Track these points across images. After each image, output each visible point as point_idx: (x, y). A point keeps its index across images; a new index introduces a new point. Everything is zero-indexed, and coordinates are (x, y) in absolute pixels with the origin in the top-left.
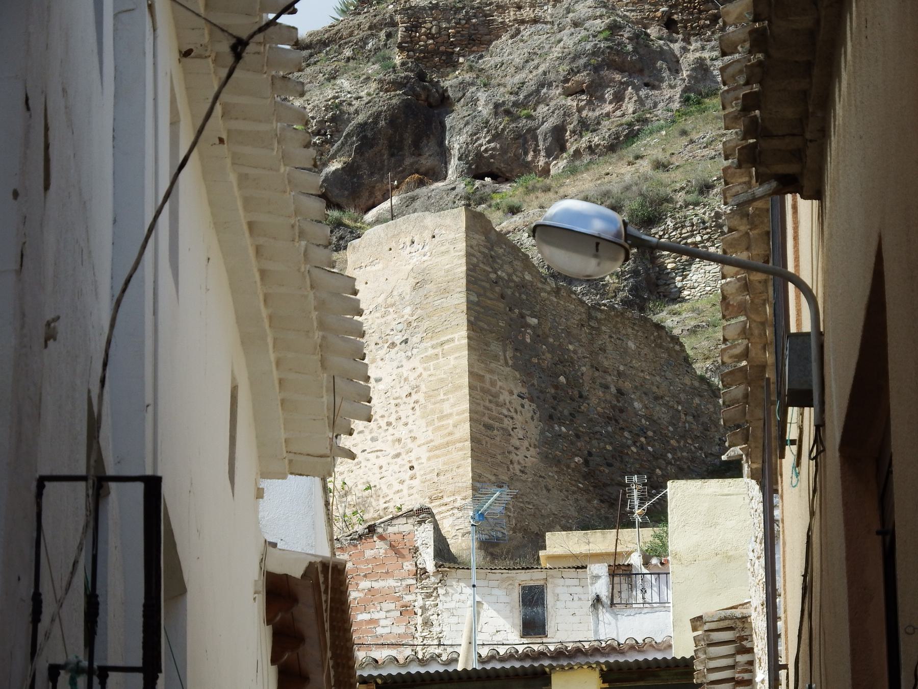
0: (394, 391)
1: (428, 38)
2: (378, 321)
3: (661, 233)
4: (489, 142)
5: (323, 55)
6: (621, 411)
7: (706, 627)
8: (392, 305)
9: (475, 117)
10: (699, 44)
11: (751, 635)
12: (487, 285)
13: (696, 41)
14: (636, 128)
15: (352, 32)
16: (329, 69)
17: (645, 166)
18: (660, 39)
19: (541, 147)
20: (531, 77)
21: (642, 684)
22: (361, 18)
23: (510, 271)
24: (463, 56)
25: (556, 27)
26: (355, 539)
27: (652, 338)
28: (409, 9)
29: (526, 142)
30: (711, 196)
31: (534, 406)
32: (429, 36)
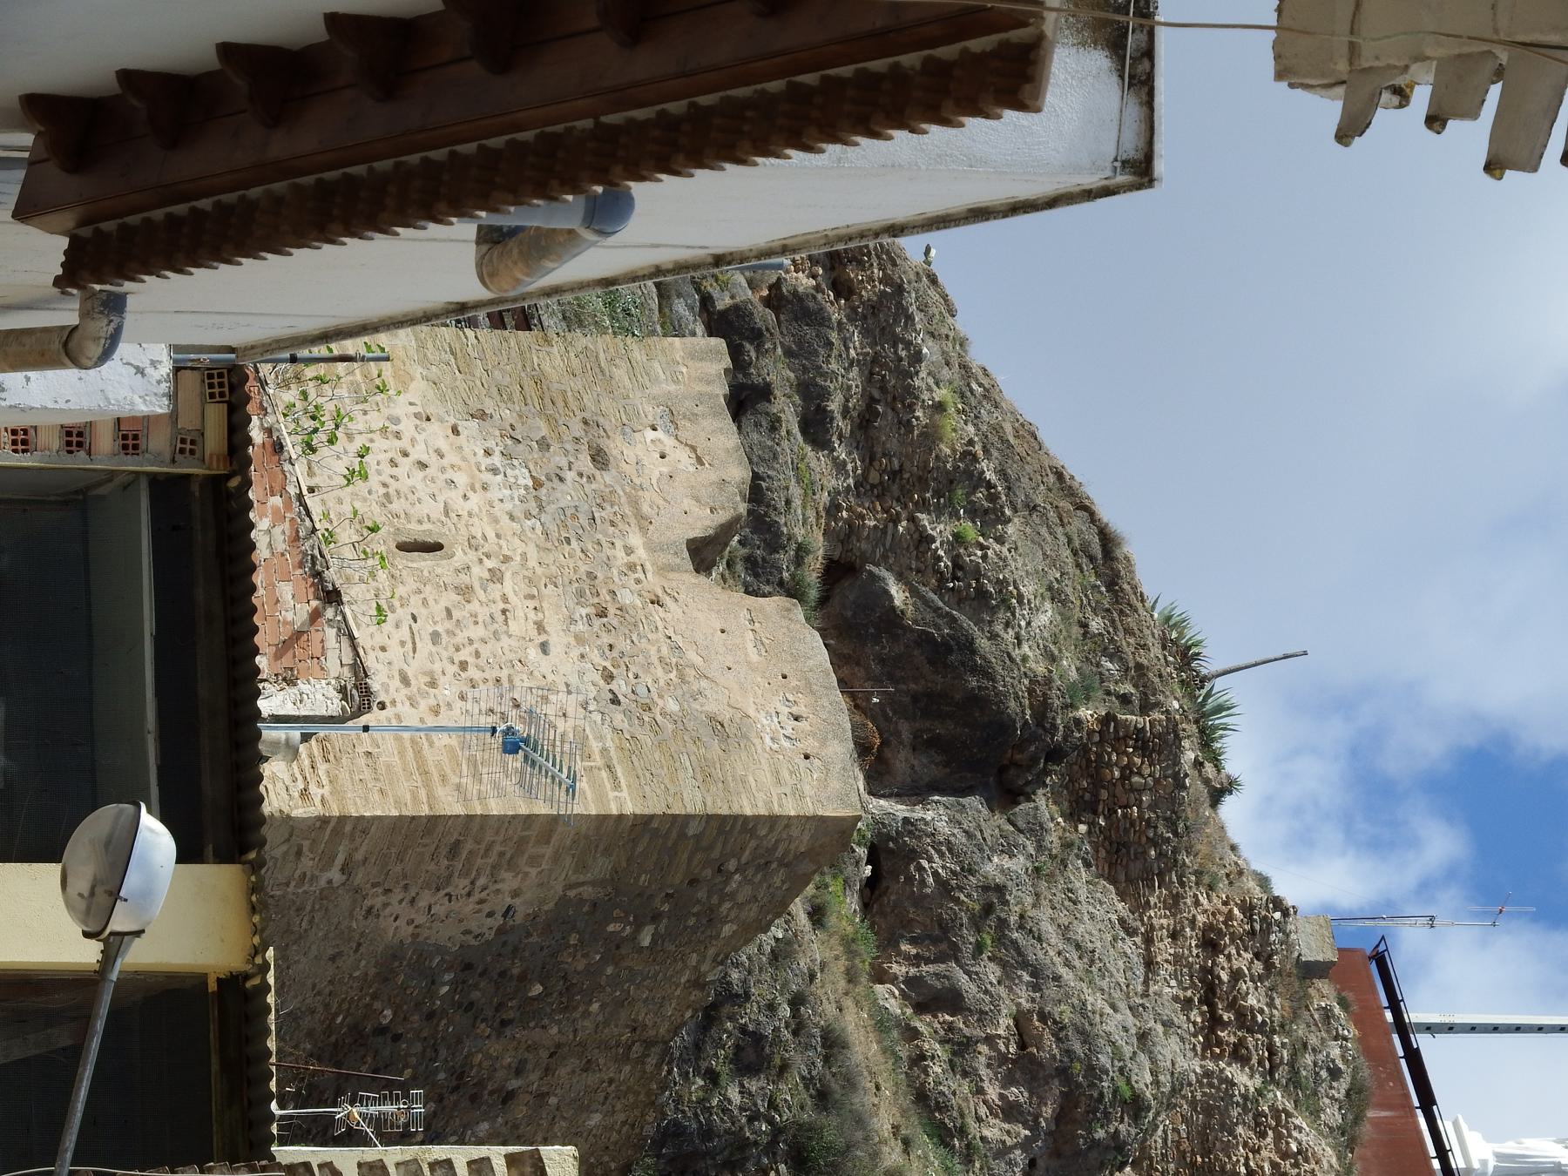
0: (525, 677)
1: (1123, 769)
2: (653, 651)
4: (936, 874)
5: (1093, 579)
6: (474, 1098)
8: (682, 677)
9: (981, 850)
12: (715, 854)
14: (956, 1142)
15: (1134, 634)
16: (1069, 590)
19: (924, 968)
20: (1050, 953)
21: (215, 1066)
22: (1156, 651)
23: (740, 898)
24: (1089, 832)
26: (314, 564)
27: (606, 1158)
29: (935, 941)
31: (490, 936)
32: (1127, 772)
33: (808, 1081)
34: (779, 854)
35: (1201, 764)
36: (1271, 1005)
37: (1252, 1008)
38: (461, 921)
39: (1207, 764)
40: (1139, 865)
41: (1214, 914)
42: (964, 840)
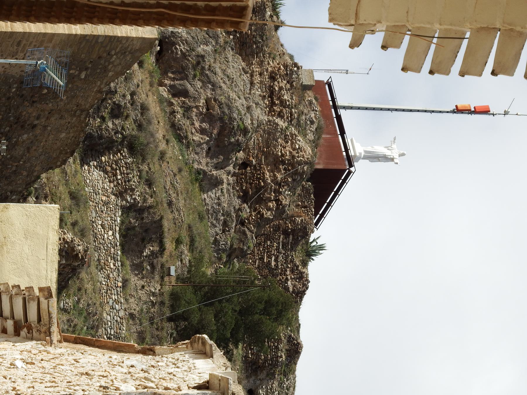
3: (124, 154)
4: (181, 51)
6: (22, 127)
7: (42, 299)
9: (197, 43)
10: (231, 182)
11: (32, 339)
12: (108, 48)
13: (233, 180)
17: (162, 146)
18: (236, 159)
19: (176, 82)
20: (219, 78)
23: (115, 64)
24: (234, 38)
25: (248, 96)
27: (66, 148)
28: (265, 7)
29: (180, 73)
30: (144, 186)
33: (135, 121)
34: (129, 49)
35: (272, 16)
36: (292, 99)
37: (285, 100)
38: (20, 67)
39: (274, 16)
40: (250, 50)
41: (274, 68)
42: (191, 39)
